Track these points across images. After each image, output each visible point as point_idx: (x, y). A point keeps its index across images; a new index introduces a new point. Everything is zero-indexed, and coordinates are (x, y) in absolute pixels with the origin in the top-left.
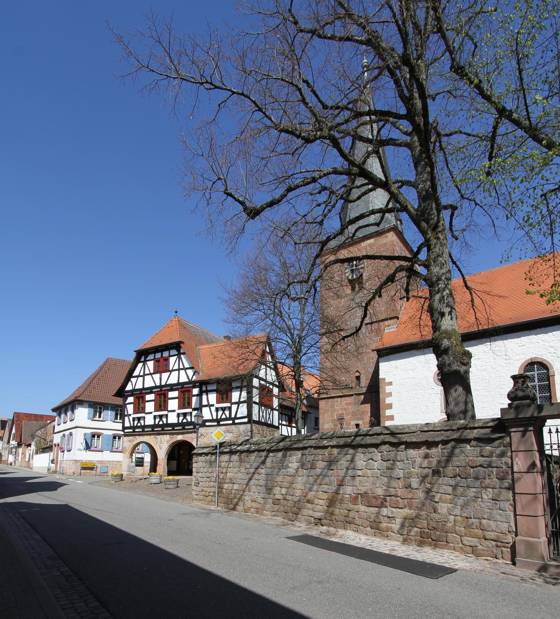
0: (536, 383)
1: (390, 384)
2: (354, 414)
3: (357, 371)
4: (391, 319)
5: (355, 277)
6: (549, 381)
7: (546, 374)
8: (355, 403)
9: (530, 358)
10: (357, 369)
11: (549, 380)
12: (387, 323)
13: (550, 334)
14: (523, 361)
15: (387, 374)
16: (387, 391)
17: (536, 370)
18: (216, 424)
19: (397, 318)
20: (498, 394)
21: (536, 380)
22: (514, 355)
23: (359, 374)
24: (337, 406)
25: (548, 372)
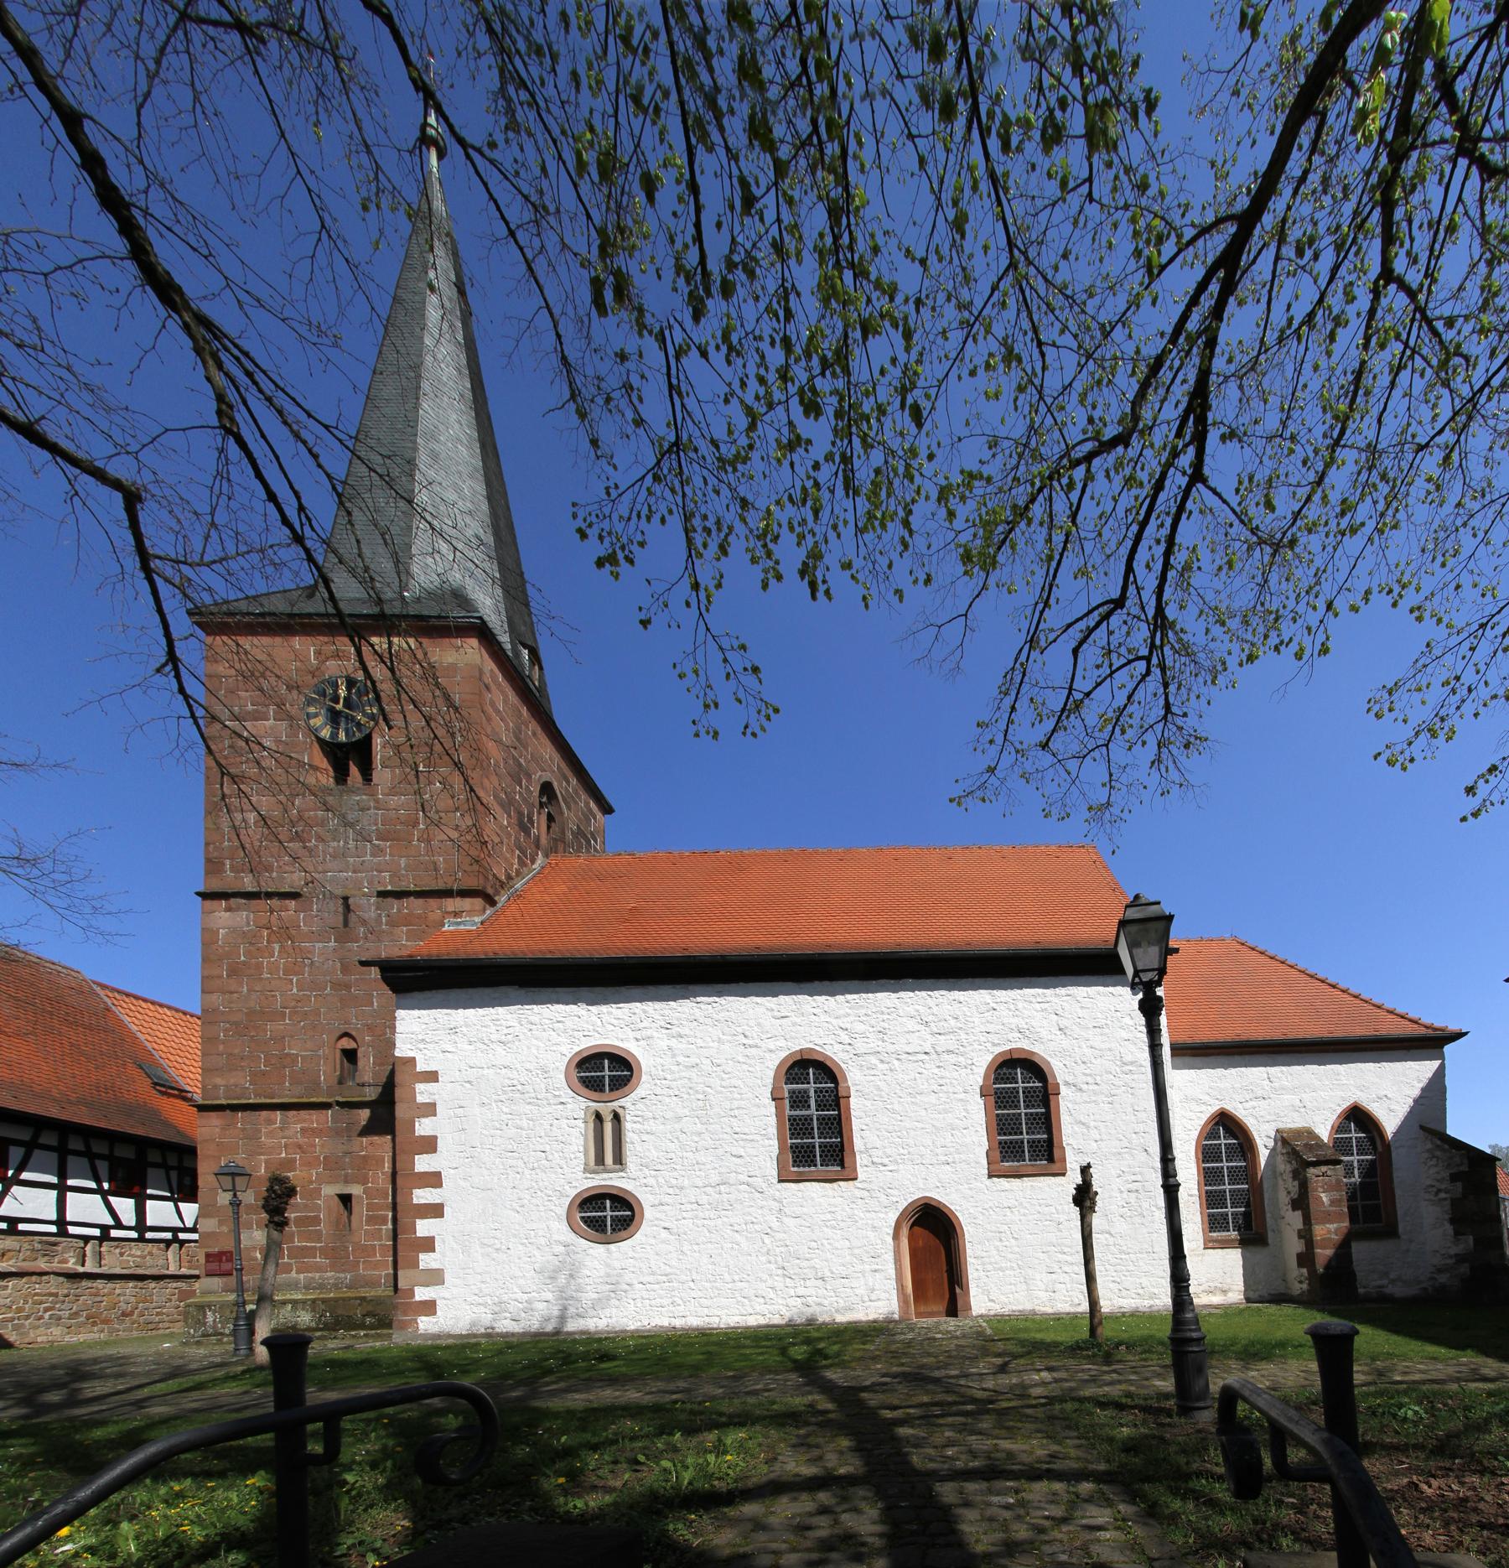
0: (813, 1111)
1: (432, 1077)
3: (346, 1035)
5: (342, 737)
8: (337, 1133)
12: (451, 904)
13: (840, 998)
14: (783, 1055)
15: (421, 1046)
16: (420, 1099)
18: (21, 1227)
19: (492, 902)
20: (728, 1130)
23: (353, 1045)
24: (270, 1134)
25: (836, 1088)
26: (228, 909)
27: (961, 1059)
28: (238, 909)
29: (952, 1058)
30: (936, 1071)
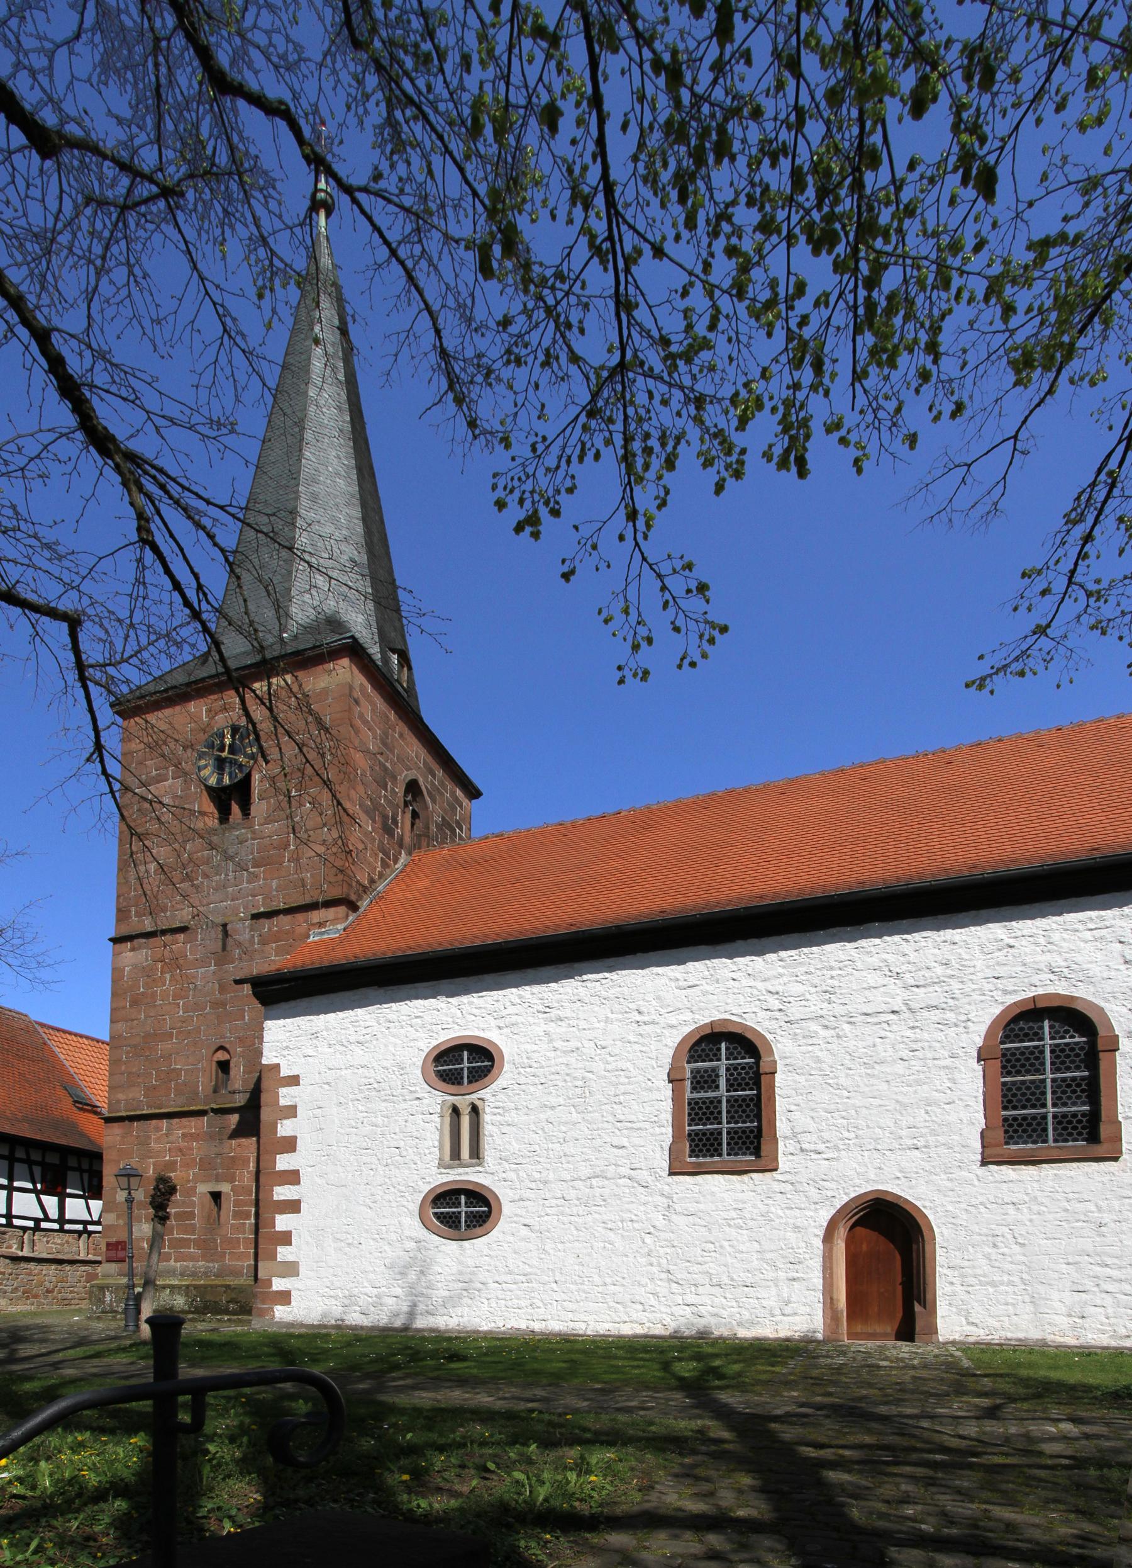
1: (294, 1080)
2: (207, 1166)
3: (222, 1048)
4: (328, 904)
5: (227, 781)
6: (759, 1089)
7: (751, 1068)
8: (211, 1137)
9: (707, 1021)
10: (220, 1042)
11: (757, 1084)
12: (316, 916)
13: (771, 957)
14: (687, 1030)
15: (285, 1053)
16: (283, 1102)
17: (723, 1056)
20: (610, 1118)
21: (723, 1082)
22: (663, 1011)
23: (226, 1057)
25: (757, 1063)
26: (133, 949)
27: (950, 1015)
28: (140, 948)
29: (935, 1016)
30: (909, 1033)
